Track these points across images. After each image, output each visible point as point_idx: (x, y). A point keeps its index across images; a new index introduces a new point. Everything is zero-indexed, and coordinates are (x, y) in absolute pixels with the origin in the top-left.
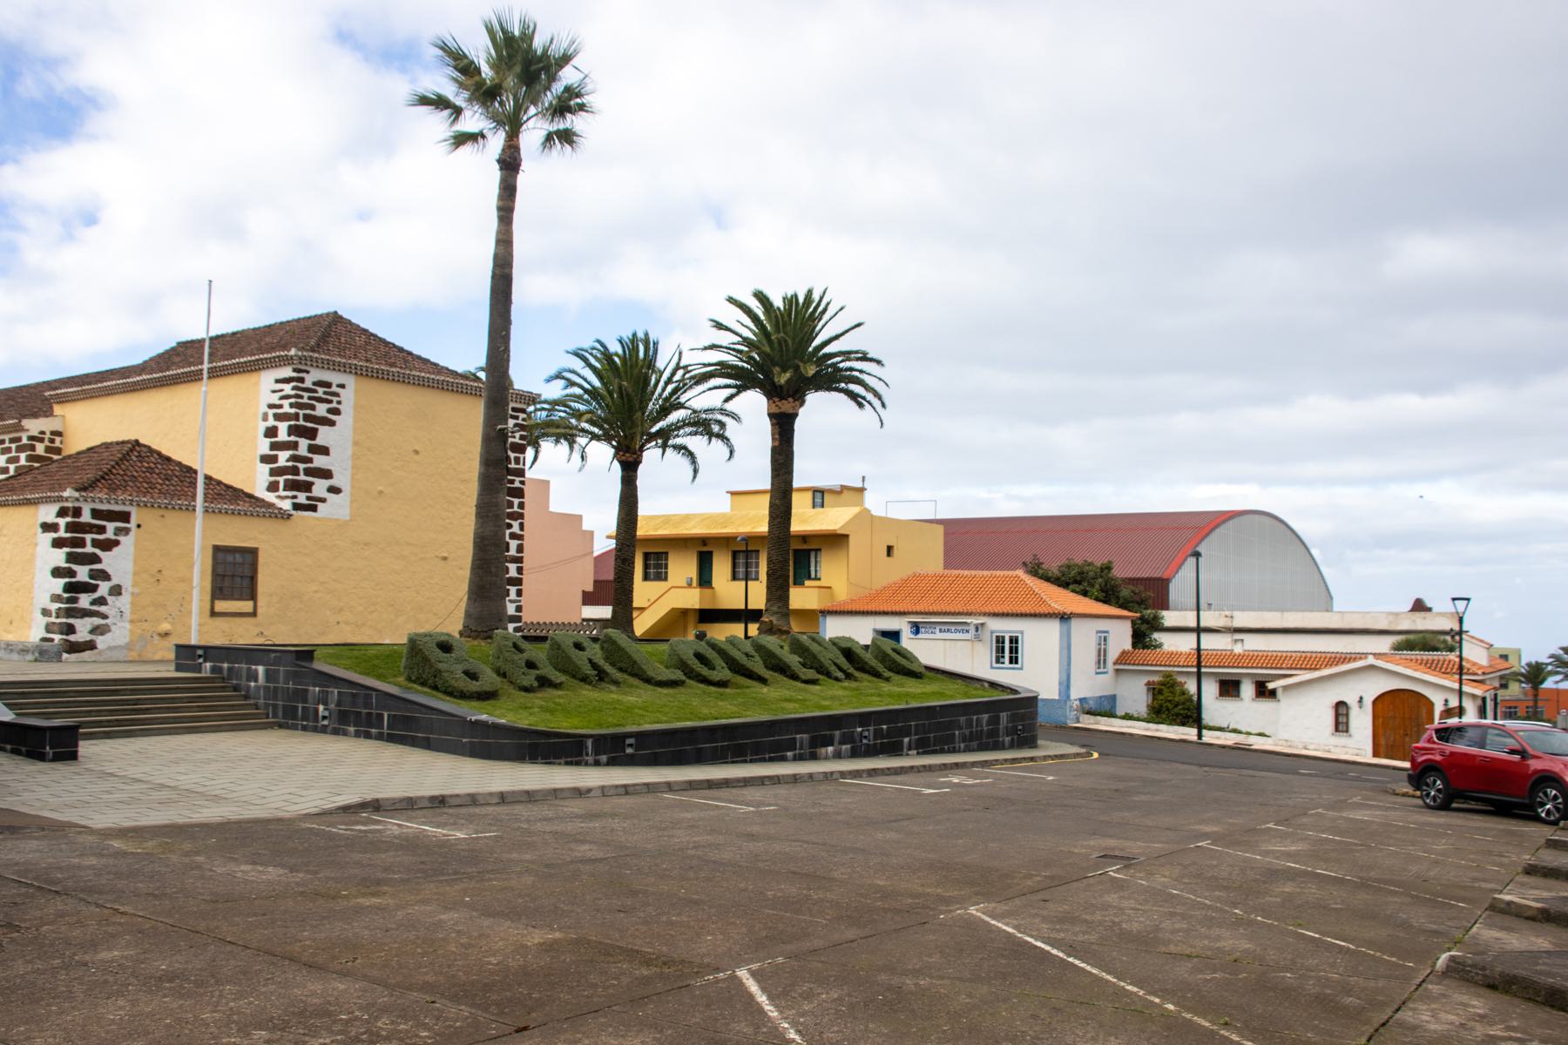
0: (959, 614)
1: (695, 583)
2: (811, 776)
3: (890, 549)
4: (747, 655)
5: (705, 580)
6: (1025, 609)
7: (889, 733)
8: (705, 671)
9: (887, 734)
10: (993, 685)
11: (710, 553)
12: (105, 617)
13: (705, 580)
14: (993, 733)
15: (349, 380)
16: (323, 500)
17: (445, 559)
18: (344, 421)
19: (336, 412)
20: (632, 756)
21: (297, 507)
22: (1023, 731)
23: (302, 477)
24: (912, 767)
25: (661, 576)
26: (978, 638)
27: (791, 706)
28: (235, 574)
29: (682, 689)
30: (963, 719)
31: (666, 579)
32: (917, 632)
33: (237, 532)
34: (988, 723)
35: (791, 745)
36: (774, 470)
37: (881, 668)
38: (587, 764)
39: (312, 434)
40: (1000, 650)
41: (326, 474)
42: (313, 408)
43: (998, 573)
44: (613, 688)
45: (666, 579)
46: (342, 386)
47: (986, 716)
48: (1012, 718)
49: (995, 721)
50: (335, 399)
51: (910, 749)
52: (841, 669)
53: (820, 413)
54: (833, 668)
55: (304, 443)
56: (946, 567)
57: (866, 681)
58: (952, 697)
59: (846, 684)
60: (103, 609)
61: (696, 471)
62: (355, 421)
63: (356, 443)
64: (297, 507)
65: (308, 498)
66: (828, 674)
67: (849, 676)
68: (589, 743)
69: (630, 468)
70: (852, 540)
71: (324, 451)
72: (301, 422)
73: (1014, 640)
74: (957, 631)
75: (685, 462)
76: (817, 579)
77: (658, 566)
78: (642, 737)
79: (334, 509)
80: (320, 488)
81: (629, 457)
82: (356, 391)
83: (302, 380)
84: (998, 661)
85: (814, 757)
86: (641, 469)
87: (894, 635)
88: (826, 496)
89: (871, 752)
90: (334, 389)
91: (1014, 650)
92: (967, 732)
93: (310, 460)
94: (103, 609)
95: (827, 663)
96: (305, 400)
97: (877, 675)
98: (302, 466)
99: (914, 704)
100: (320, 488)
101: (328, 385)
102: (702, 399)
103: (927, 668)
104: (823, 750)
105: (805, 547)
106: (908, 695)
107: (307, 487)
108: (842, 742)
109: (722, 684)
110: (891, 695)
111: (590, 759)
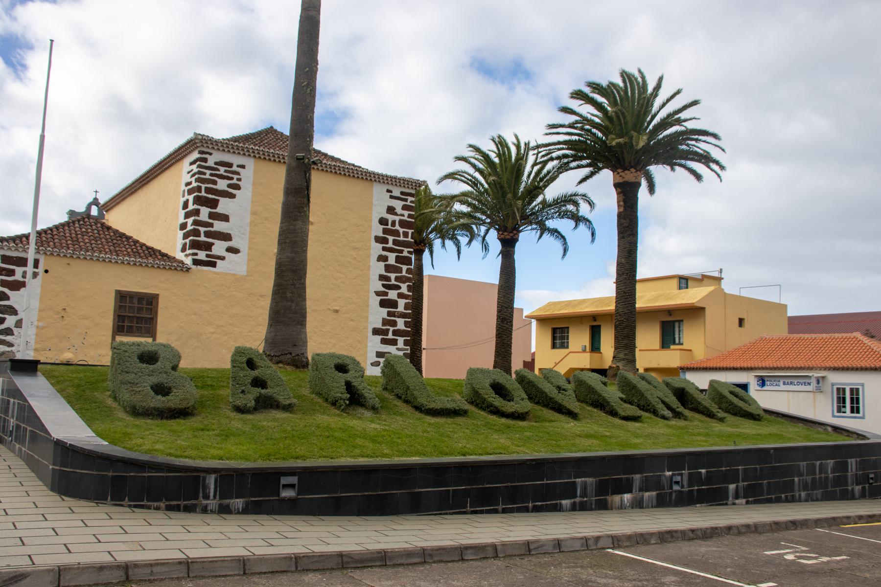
0: (801, 369)
1: (588, 350)
2: (558, 544)
3: (741, 322)
4: (559, 388)
5: (595, 346)
6: (864, 364)
7: (709, 479)
8: (498, 402)
9: (708, 480)
10: (836, 429)
11: (599, 327)
12: (10, 345)
13: (595, 346)
14: (841, 481)
15: (249, 163)
16: (222, 258)
17: (337, 311)
18: (244, 195)
19: (237, 187)
20: (291, 500)
21: (196, 262)
22: (876, 479)
23: (203, 238)
24: (729, 528)
25: (564, 346)
26: (819, 390)
27: (588, 442)
28: (135, 313)
29: (460, 420)
30: (803, 464)
31: (567, 347)
32: (763, 385)
33: (138, 280)
34: (834, 470)
35: (569, 491)
36: (620, 233)
37: (714, 408)
38: (205, 510)
39: (214, 204)
40: (841, 400)
41: (226, 237)
42: (215, 183)
43: (837, 335)
44: (368, 414)
45: (567, 347)
46: (243, 167)
47: (831, 462)
48: (862, 465)
49: (842, 467)
50: (236, 177)
51: (737, 497)
52: (669, 407)
53: (669, 193)
54: (660, 407)
55: (205, 212)
56: (790, 332)
57: (697, 421)
58: (790, 440)
59: (673, 422)
60: (9, 338)
61: (565, 250)
62: (253, 195)
63: (254, 213)
64: (196, 262)
65: (207, 256)
66: (655, 412)
67: (677, 415)
68: (211, 480)
69: (508, 245)
70: (707, 311)
71: (225, 218)
72: (203, 194)
73: (855, 392)
74: (799, 384)
75: (558, 245)
76: (680, 344)
77: (562, 338)
78: (311, 478)
79: (230, 265)
80: (219, 248)
81: (507, 235)
82: (255, 171)
83: (205, 160)
84: (839, 411)
85: (603, 506)
86: (518, 246)
87: (744, 387)
88: (690, 283)
89: (685, 500)
90: (235, 168)
91: (855, 400)
92: (809, 479)
93: (211, 225)
94: (9, 338)
95: (654, 401)
96: (207, 176)
97: (711, 415)
98: (202, 230)
99: (744, 446)
100: (219, 248)
101: (230, 165)
102: (564, 184)
103: (766, 411)
104: (617, 498)
105: (671, 319)
106: (739, 435)
107: (208, 247)
108: (644, 488)
109: (520, 416)
110: (720, 436)
111: (212, 503)
